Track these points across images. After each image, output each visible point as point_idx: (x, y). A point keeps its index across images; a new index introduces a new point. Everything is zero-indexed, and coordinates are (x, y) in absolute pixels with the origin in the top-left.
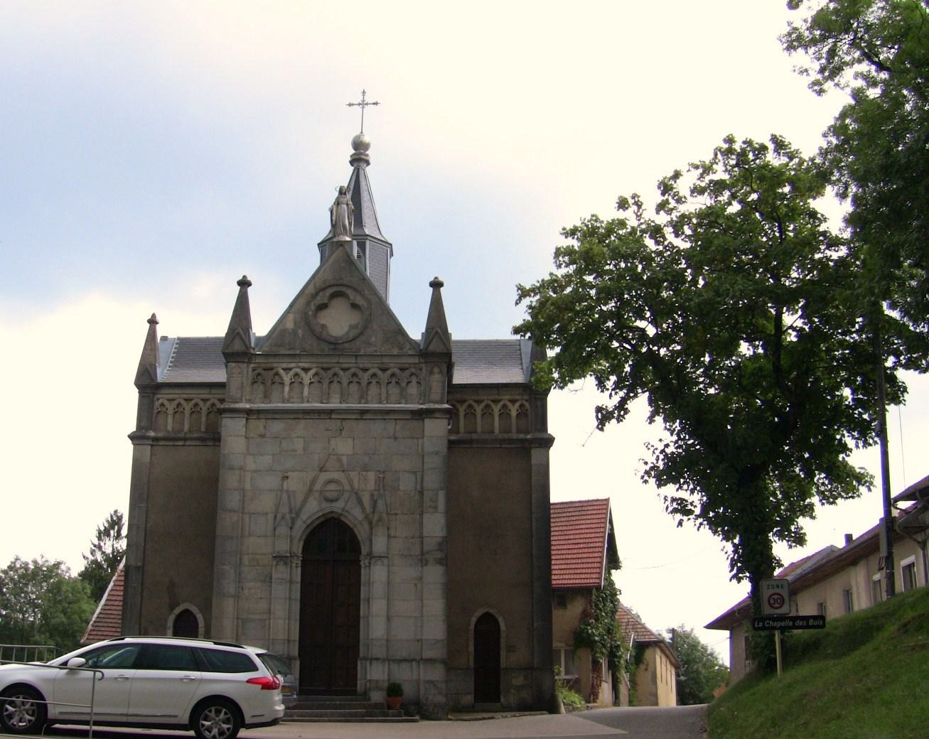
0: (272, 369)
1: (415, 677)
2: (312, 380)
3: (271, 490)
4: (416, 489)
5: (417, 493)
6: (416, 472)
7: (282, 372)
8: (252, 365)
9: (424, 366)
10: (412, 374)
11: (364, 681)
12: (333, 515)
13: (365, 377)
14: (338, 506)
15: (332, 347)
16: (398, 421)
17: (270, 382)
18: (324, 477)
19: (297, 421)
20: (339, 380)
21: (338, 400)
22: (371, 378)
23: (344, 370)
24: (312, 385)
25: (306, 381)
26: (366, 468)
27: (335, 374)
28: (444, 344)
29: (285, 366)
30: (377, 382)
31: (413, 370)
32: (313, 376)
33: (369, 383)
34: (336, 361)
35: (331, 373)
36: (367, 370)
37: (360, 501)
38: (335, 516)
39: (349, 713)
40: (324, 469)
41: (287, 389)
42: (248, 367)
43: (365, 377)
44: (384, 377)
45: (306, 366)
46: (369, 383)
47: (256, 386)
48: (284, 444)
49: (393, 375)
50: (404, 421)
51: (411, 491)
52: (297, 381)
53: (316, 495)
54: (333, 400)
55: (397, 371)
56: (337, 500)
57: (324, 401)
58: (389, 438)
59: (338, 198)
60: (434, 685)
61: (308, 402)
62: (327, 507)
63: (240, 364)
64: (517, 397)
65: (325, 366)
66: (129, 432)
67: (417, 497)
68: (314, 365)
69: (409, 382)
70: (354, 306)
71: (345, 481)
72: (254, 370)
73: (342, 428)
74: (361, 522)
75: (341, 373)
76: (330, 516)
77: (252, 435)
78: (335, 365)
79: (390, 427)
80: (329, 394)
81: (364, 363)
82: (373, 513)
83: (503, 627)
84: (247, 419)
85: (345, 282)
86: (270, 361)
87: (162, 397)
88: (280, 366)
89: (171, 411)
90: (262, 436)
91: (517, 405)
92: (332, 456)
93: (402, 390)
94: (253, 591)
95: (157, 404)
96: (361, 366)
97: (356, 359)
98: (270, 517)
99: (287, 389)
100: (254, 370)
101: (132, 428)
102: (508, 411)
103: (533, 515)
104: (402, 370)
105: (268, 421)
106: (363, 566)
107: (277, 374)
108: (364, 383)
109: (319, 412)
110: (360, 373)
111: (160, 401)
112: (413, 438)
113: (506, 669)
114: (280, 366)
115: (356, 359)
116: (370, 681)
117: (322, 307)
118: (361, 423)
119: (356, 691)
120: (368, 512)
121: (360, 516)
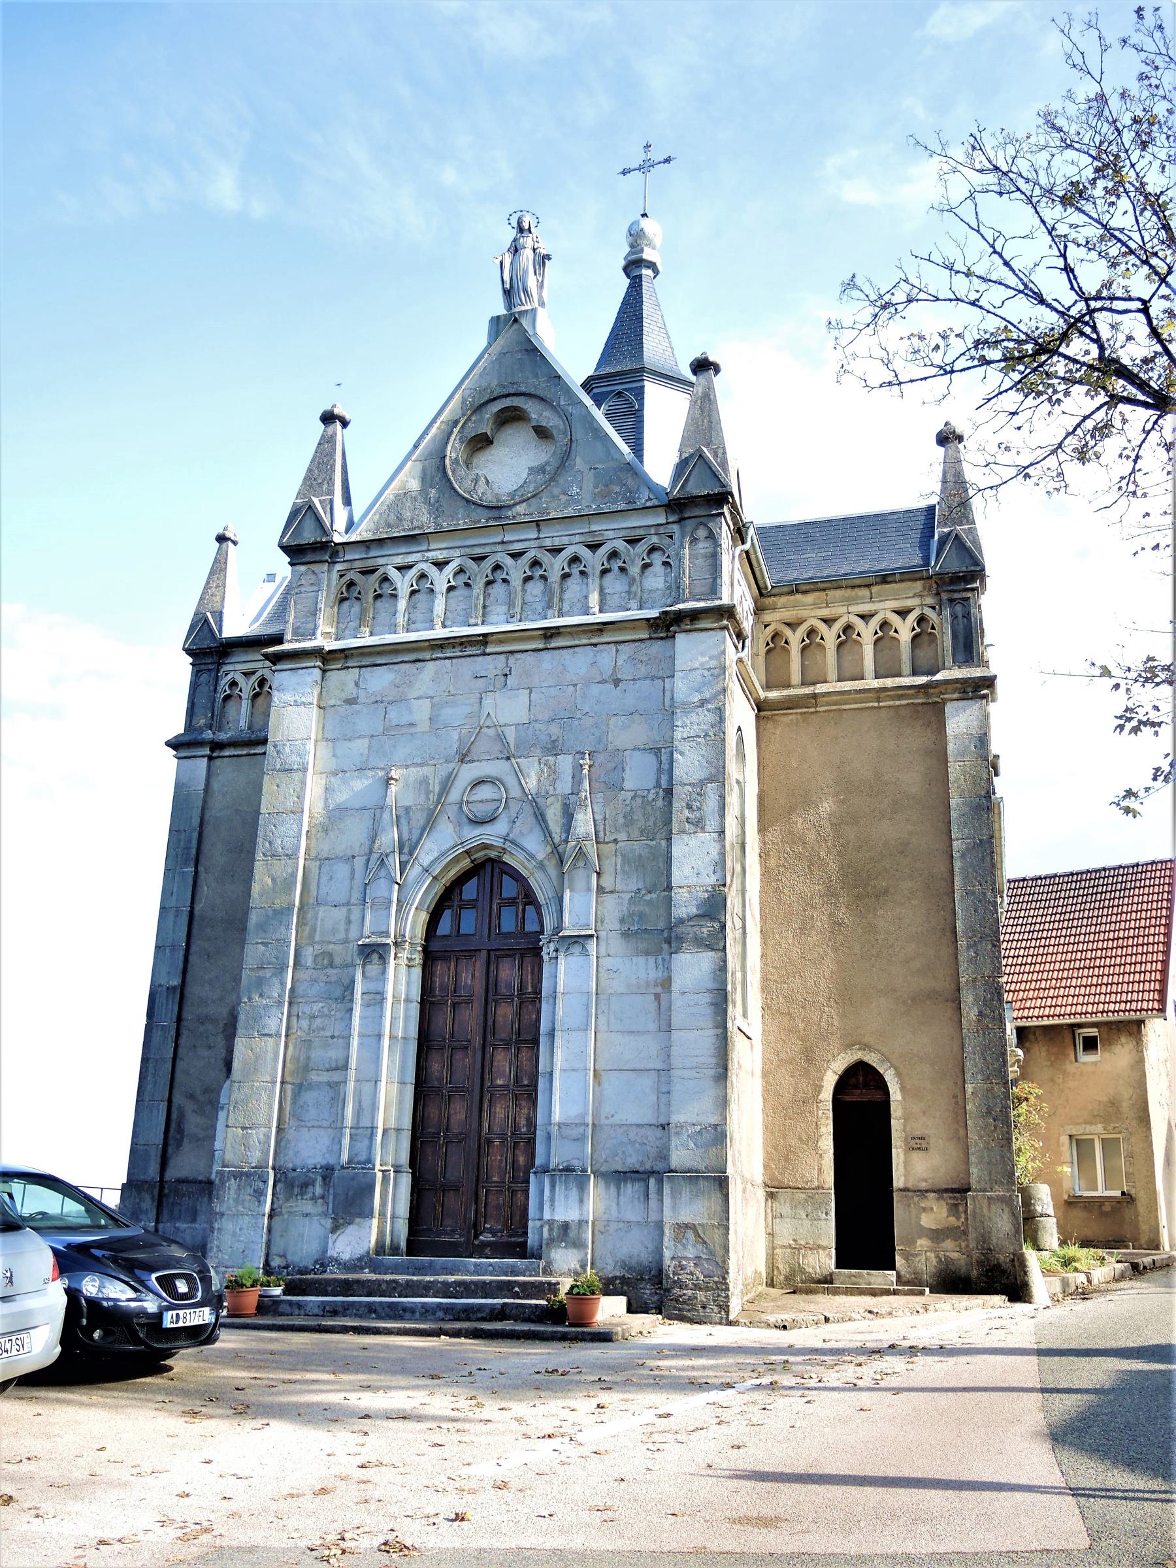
0: (373, 571)
1: (654, 1217)
2: (453, 583)
3: (364, 809)
4: (658, 784)
5: (661, 793)
6: (659, 749)
7: (394, 574)
8: (338, 567)
9: (675, 528)
10: (653, 549)
11: (538, 1223)
12: (487, 852)
13: (556, 566)
14: (493, 834)
15: (495, 513)
16: (621, 647)
17: (371, 595)
18: (469, 773)
19: (419, 665)
20: (504, 576)
21: (503, 617)
22: (569, 565)
23: (515, 556)
24: (452, 594)
25: (441, 586)
26: (553, 748)
27: (497, 567)
28: (715, 475)
29: (399, 560)
30: (582, 573)
31: (655, 539)
32: (456, 574)
33: (565, 576)
34: (499, 540)
35: (488, 564)
36: (560, 550)
37: (540, 817)
38: (493, 854)
39: (448, 1309)
40: (467, 759)
41: (402, 604)
42: (329, 571)
43: (556, 566)
44: (594, 561)
45: (440, 556)
46: (565, 576)
47: (346, 604)
48: (393, 714)
49: (614, 555)
50: (633, 645)
51: (649, 791)
52: (422, 589)
53: (452, 811)
54: (492, 618)
55: (621, 545)
56: (492, 820)
57: (472, 621)
58: (603, 682)
59: (515, 240)
60: (698, 1235)
61: (444, 626)
62: (474, 835)
63: (314, 567)
64: (909, 603)
65: (478, 551)
66: (170, 736)
67: (660, 803)
68: (457, 553)
69: (646, 566)
70: (542, 433)
71: (511, 781)
72: (341, 576)
73: (507, 671)
74: (541, 866)
75: (509, 561)
76: (480, 855)
77: (332, 702)
78: (500, 548)
79: (606, 658)
80: (484, 607)
81: (552, 536)
82: (567, 841)
83: (895, 1094)
84: (324, 671)
85: (523, 389)
86: (372, 554)
87: (234, 669)
88: (388, 563)
89: (246, 694)
90: (351, 701)
91: (912, 617)
92: (485, 730)
93: (632, 582)
94: (318, 1022)
95: (224, 682)
96: (548, 543)
97: (539, 531)
98: (359, 862)
99: (402, 604)
100: (341, 576)
101: (177, 727)
102: (892, 633)
103: (955, 843)
104: (632, 542)
105: (364, 669)
106: (545, 958)
107: (385, 579)
108: (554, 576)
109: (462, 642)
110: (546, 558)
111: (229, 677)
112: (653, 678)
113: (906, 1190)
114: (388, 563)
115: (539, 531)
116: (551, 1222)
117: (480, 443)
118: (546, 655)
119: (524, 1244)
120: (557, 840)
121: (541, 851)
